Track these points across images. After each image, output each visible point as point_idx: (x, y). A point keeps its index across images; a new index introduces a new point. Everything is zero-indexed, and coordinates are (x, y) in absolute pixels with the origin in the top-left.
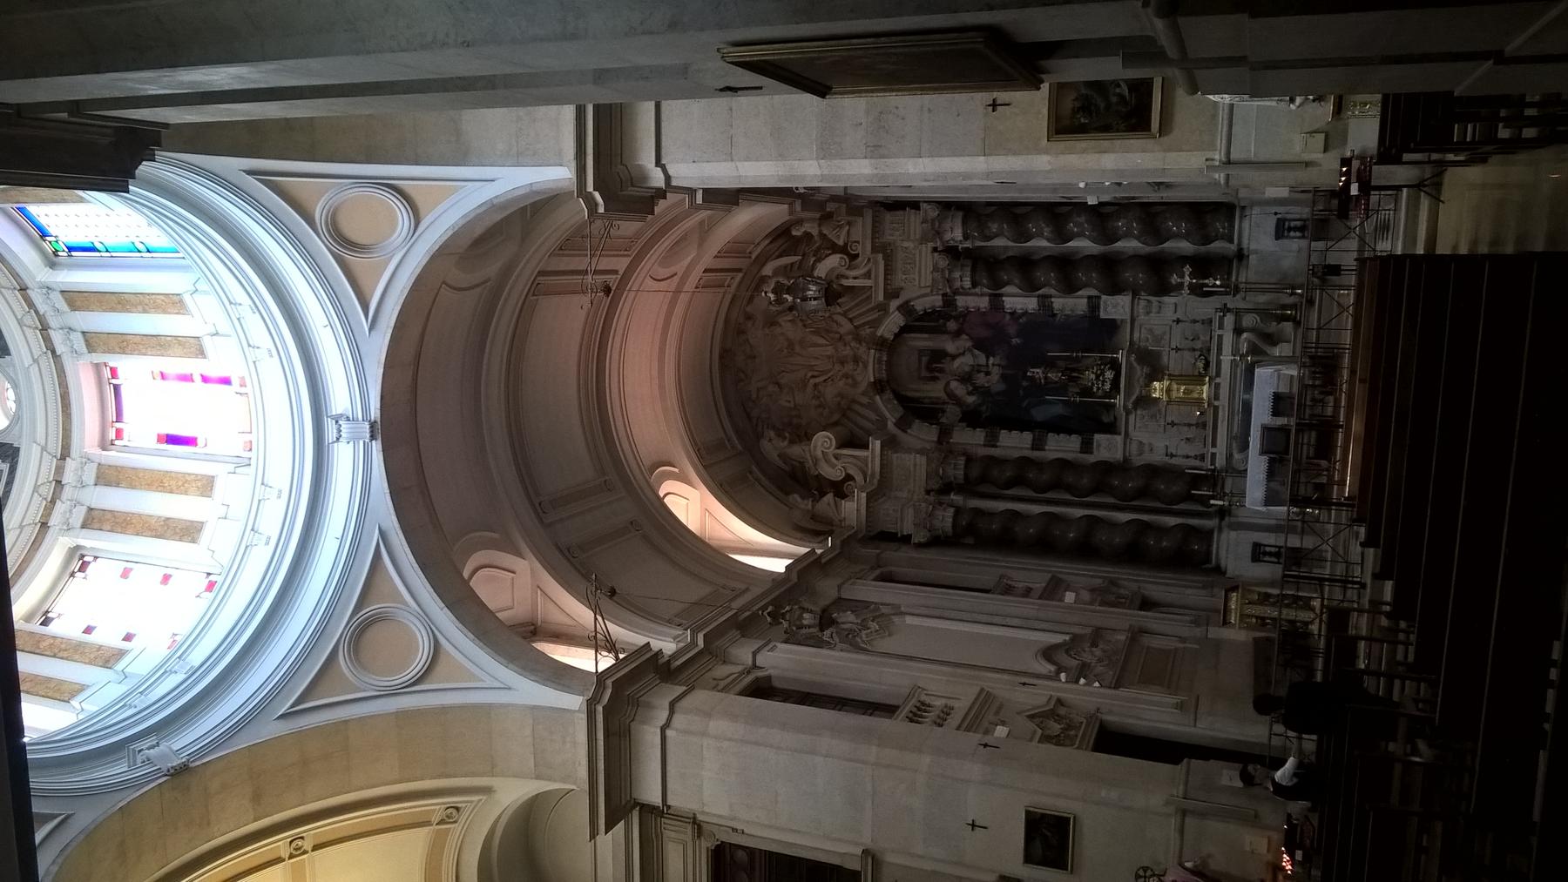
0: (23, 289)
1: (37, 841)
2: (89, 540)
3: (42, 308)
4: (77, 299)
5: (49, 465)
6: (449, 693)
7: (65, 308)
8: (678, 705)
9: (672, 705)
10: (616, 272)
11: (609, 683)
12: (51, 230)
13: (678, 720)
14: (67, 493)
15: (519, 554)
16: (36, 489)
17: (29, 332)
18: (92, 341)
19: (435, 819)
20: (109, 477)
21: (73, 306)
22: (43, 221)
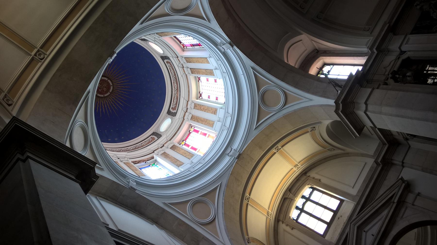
0: (178, 57)
1: (69, 147)
2: (193, 124)
3: (182, 62)
4: (189, 60)
5: (185, 102)
6: (289, 108)
7: (186, 62)
8: (368, 102)
9: (366, 103)
10: (288, 61)
11: (340, 102)
12: (182, 41)
13: (370, 108)
14: (188, 111)
15: (301, 34)
16: (182, 109)
17: (175, 58)
18: (193, 71)
19: (309, 130)
20: (197, 106)
21: (188, 62)
22: (180, 39)
